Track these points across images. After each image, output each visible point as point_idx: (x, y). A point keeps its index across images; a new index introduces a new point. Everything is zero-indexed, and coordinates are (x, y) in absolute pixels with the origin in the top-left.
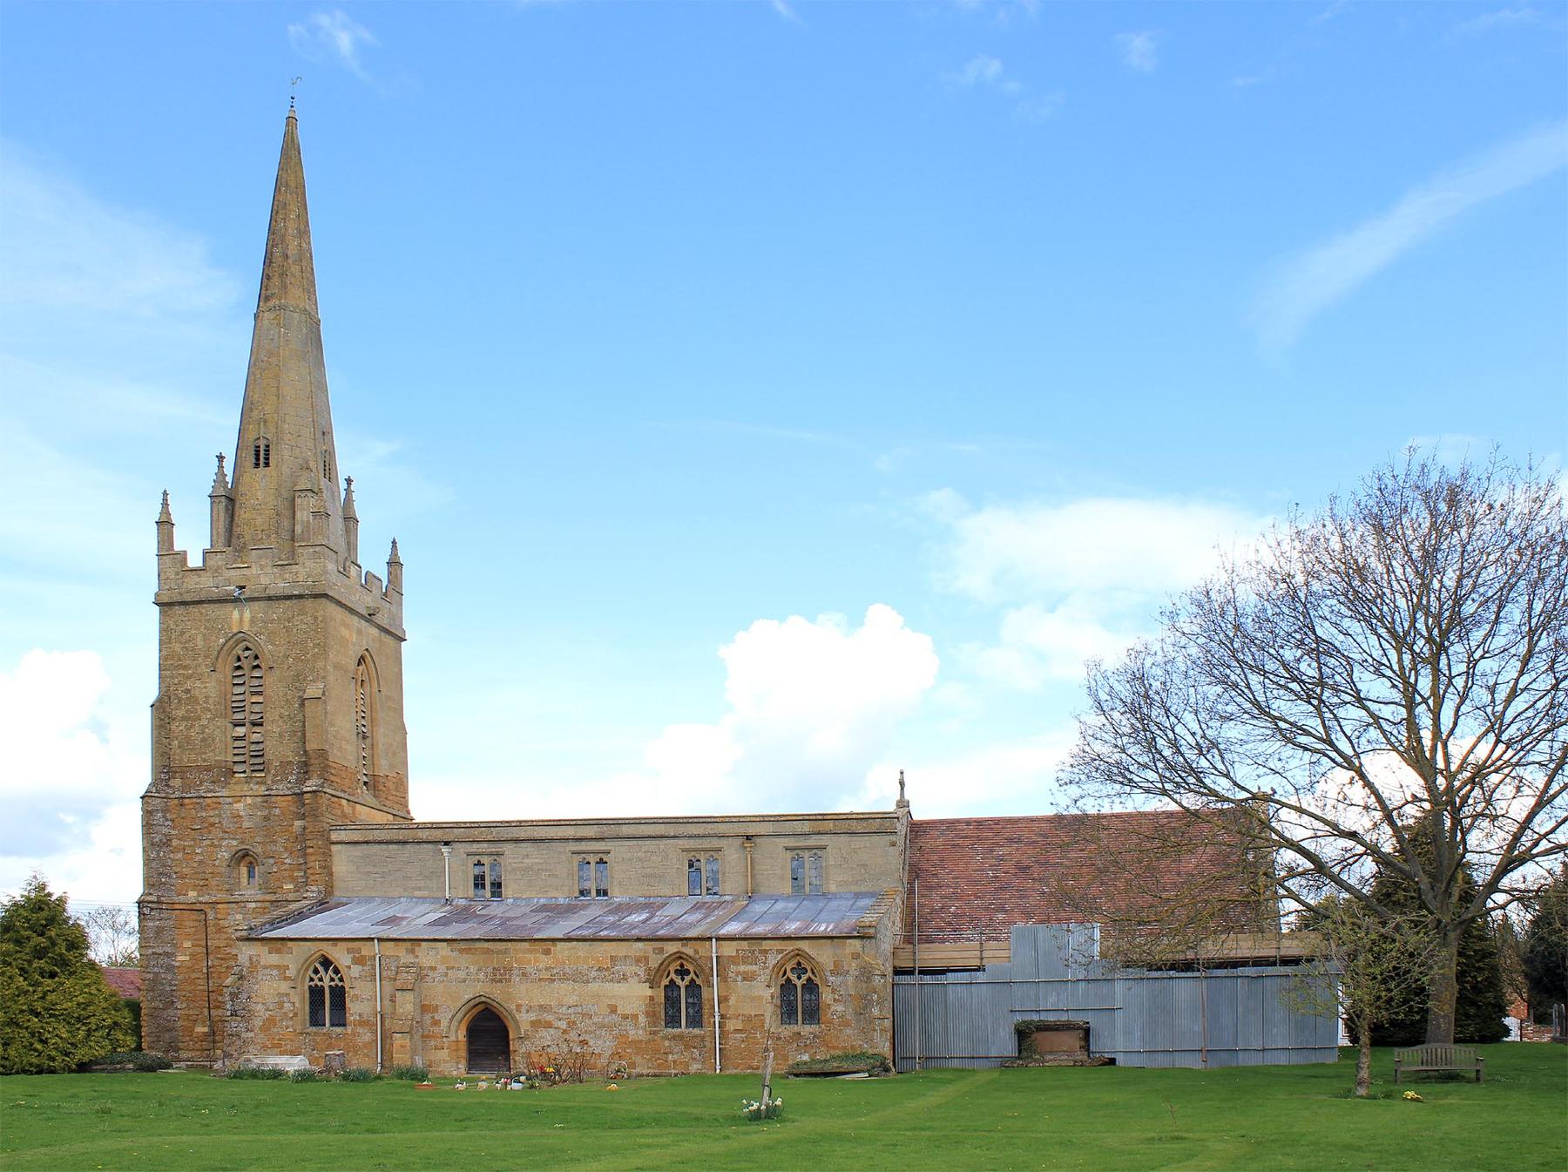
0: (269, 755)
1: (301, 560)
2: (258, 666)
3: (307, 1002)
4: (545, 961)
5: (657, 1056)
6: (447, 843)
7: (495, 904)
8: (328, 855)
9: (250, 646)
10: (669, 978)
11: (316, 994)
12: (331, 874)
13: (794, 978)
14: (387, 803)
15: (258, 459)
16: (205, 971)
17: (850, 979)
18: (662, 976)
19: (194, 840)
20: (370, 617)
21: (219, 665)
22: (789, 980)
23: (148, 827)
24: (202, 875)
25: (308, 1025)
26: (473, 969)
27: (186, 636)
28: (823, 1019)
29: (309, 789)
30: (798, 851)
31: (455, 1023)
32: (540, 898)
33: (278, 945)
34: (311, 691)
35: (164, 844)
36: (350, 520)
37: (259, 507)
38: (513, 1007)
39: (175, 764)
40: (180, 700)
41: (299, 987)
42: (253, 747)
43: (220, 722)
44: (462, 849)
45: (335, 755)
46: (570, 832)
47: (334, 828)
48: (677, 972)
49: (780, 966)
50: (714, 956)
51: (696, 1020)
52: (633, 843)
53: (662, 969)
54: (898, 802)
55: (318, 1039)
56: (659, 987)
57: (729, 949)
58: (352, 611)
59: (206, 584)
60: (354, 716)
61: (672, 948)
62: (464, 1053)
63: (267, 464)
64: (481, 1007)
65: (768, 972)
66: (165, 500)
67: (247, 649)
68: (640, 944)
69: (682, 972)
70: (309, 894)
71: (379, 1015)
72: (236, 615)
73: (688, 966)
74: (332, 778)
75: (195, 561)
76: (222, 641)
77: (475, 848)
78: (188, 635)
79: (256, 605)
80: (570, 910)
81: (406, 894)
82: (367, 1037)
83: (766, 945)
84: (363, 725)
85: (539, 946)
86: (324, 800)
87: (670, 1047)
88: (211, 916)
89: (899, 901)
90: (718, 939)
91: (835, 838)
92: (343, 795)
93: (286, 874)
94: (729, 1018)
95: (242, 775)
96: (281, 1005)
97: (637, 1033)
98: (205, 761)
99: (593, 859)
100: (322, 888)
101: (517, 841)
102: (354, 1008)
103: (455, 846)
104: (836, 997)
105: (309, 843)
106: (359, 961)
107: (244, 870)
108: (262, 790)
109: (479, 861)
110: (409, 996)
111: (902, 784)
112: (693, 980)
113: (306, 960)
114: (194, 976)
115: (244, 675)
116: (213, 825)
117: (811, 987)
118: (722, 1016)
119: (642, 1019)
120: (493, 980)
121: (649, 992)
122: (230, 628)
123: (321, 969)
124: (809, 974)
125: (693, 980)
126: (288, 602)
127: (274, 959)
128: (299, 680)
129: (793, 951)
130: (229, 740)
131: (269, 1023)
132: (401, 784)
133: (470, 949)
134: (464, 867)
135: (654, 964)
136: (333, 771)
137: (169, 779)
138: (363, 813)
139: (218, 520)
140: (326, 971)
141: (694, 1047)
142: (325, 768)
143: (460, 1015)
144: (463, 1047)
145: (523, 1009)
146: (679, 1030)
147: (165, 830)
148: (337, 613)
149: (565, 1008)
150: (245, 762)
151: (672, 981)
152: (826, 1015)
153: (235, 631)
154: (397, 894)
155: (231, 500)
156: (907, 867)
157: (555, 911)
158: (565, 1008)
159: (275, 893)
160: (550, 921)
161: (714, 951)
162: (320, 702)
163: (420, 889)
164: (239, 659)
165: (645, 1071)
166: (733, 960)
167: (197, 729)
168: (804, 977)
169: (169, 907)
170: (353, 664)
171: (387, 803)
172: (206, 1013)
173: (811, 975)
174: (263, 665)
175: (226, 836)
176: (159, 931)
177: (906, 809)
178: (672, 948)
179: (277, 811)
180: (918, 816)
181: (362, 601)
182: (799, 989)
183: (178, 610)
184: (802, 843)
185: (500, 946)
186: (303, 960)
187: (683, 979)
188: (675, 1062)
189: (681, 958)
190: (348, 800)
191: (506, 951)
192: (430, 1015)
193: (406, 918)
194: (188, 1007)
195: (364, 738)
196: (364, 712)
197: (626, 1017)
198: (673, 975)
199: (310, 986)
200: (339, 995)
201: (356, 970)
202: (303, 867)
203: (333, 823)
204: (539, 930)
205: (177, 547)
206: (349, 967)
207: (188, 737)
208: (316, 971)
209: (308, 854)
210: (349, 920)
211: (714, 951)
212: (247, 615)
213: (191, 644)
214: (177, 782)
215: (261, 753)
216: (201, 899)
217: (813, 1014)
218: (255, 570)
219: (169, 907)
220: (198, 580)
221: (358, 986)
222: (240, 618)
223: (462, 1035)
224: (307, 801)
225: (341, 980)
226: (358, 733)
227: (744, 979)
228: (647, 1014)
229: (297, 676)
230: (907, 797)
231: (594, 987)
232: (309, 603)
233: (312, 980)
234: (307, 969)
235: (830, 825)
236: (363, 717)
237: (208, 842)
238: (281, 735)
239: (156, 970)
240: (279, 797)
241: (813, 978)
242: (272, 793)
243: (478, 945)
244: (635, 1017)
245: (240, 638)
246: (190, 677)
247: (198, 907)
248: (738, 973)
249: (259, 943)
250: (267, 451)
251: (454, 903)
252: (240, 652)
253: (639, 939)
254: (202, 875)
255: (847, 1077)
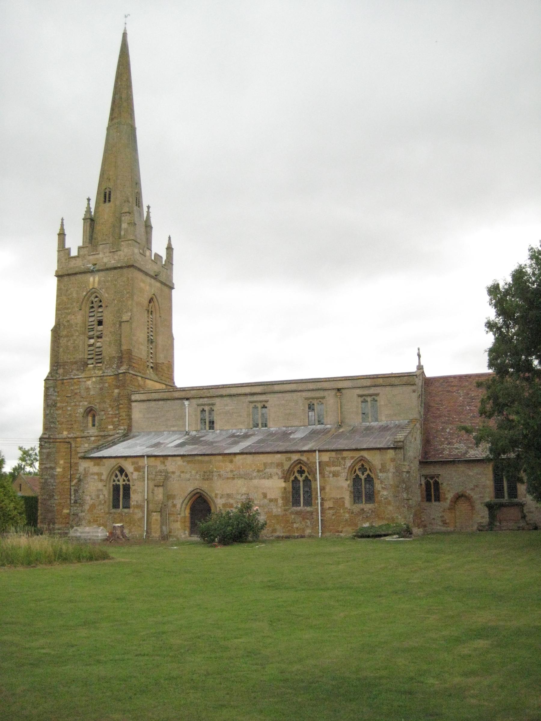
0: (104, 354)
1: (122, 248)
2: (101, 306)
3: (112, 493)
4: (230, 466)
5: (288, 525)
6: (187, 399)
7: (210, 434)
8: (130, 408)
9: (98, 296)
10: (294, 476)
11: (116, 488)
12: (130, 419)
13: (360, 474)
14: (163, 378)
15: (105, 199)
16: (69, 477)
17: (390, 475)
18: (290, 475)
19: (67, 402)
20: (155, 277)
21: (83, 307)
22: (357, 476)
23: (47, 396)
24: (70, 423)
25: (111, 508)
26: (193, 472)
27: (69, 292)
28: (376, 499)
29: (122, 371)
30: (320, 400)
31: (184, 506)
32: (233, 430)
33: (98, 461)
34: (125, 318)
35: (53, 406)
36: (148, 227)
37: (105, 223)
38: (213, 495)
39: (61, 361)
40: (64, 326)
41: (108, 485)
42: (97, 350)
43: (82, 337)
44: (194, 402)
45: (136, 353)
46: (247, 390)
47: (133, 393)
48: (298, 471)
49: (352, 468)
50: (317, 461)
51: (309, 502)
52: (280, 395)
53: (290, 471)
54: (417, 366)
55: (116, 516)
56: (289, 481)
57: (325, 457)
58: (147, 274)
59: (79, 264)
60: (146, 330)
61: (295, 457)
62: (188, 524)
63: (109, 201)
64: (197, 495)
65: (346, 470)
66: (62, 222)
67: (97, 297)
68: (279, 456)
69: (301, 472)
70: (120, 431)
71: (146, 502)
72: (91, 279)
73: (304, 468)
74: (134, 365)
75: (74, 253)
76: (85, 293)
77: (201, 401)
78: (69, 291)
79: (102, 274)
80: (246, 436)
81: (167, 429)
82: (140, 515)
83: (345, 454)
84: (152, 336)
85: (227, 458)
86: (128, 377)
87: (294, 519)
88: (73, 445)
89: (418, 425)
90: (319, 451)
91: (383, 388)
92: (139, 374)
93: (110, 420)
94: (326, 500)
95: (92, 366)
96: (98, 497)
97: (277, 510)
98: (74, 358)
99: (259, 405)
100: (126, 427)
101: (222, 396)
102: (135, 498)
103: (192, 400)
104: (383, 486)
105: (121, 402)
106: (137, 469)
107: (90, 419)
108: (100, 373)
109: (255, 406)
110: (161, 490)
111: (419, 356)
112: (306, 476)
113: (112, 469)
114: (64, 480)
115: (94, 311)
116: (76, 394)
117: (369, 480)
118: (322, 499)
119: (280, 502)
120: (203, 479)
121: (283, 485)
122: (89, 286)
123: (119, 474)
124: (368, 472)
125: (306, 476)
126: (116, 271)
127: (96, 469)
128: (119, 312)
129: (359, 458)
130: (86, 346)
131: (93, 506)
132: (170, 367)
133: (192, 460)
134: (196, 413)
135: (286, 467)
136: (134, 361)
137: (58, 369)
138: (150, 384)
139: (86, 231)
140: (121, 475)
141: (308, 519)
142: (130, 359)
143: (186, 501)
144: (188, 519)
145: (219, 497)
146: (300, 508)
147: (54, 398)
148: (140, 275)
149: (240, 495)
150: (93, 358)
151: (296, 478)
152: (378, 498)
153: (91, 287)
154: (162, 430)
155: (92, 220)
156: (423, 405)
157: (236, 439)
158: (240, 495)
159: (104, 431)
160: (236, 443)
161: (317, 458)
162: (129, 323)
163: (173, 426)
164: (92, 303)
165: (282, 535)
166: (327, 464)
167: (72, 342)
168: (366, 474)
169: (54, 440)
170: (146, 302)
171: (163, 378)
172: (69, 502)
173: (369, 472)
174: (103, 305)
175: (82, 399)
176: (49, 455)
177: (421, 371)
178: (295, 457)
179: (107, 385)
180: (429, 374)
181: (151, 268)
182: (363, 481)
183: (66, 279)
184: (366, 392)
185: (207, 458)
186: (109, 470)
187: (301, 476)
188: (297, 528)
189: (300, 463)
190: (142, 377)
191: (210, 462)
192: (172, 501)
193: (164, 443)
194: (60, 499)
195: (152, 342)
196: (152, 328)
197: (271, 500)
198: (296, 474)
199: (113, 485)
200: (127, 488)
201: (135, 475)
202: (118, 416)
203: (133, 390)
204: (227, 448)
205: (67, 246)
206: (132, 473)
207: (67, 346)
208: (116, 476)
209: (121, 408)
210: (136, 445)
211: (317, 458)
212: (97, 279)
213: (71, 296)
214: (61, 371)
215: (100, 353)
216: (69, 436)
217: (371, 497)
218: (101, 255)
219: (54, 440)
220: (75, 262)
221: (136, 484)
222: (93, 280)
223: (187, 512)
224: (121, 378)
225: (128, 480)
226: (148, 340)
227: (334, 475)
228: (283, 498)
229: (119, 310)
230: (422, 364)
231: (255, 482)
232: (125, 271)
233: (114, 481)
234: (112, 475)
235: (381, 381)
236: (152, 331)
237: (73, 404)
238: (110, 343)
239: (46, 477)
240: (108, 377)
241: (370, 474)
242: (105, 374)
243: (197, 458)
244: (276, 500)
245: (93, 292)
246: (69, 314)
247: (67, 440)
248: (330, 472)
249: (89, 460)
250: (110, 194)
251: (190, 434)
252: (93, 299)
253: (278, 452)
254: (70, 423)
255: (388, 539)
